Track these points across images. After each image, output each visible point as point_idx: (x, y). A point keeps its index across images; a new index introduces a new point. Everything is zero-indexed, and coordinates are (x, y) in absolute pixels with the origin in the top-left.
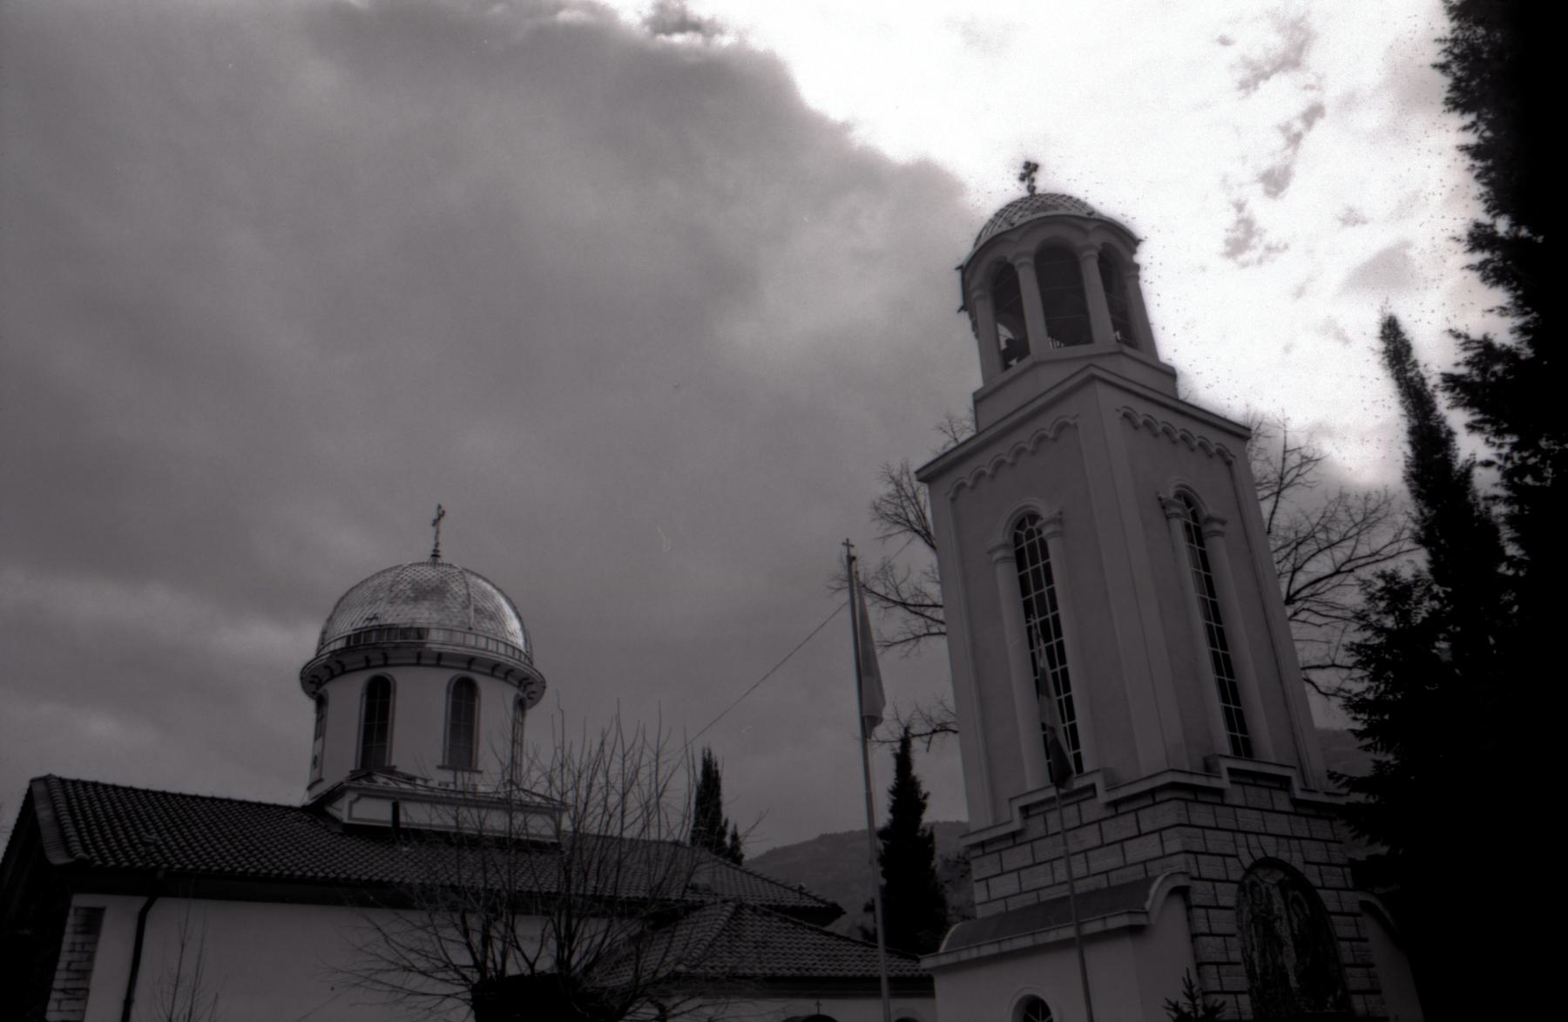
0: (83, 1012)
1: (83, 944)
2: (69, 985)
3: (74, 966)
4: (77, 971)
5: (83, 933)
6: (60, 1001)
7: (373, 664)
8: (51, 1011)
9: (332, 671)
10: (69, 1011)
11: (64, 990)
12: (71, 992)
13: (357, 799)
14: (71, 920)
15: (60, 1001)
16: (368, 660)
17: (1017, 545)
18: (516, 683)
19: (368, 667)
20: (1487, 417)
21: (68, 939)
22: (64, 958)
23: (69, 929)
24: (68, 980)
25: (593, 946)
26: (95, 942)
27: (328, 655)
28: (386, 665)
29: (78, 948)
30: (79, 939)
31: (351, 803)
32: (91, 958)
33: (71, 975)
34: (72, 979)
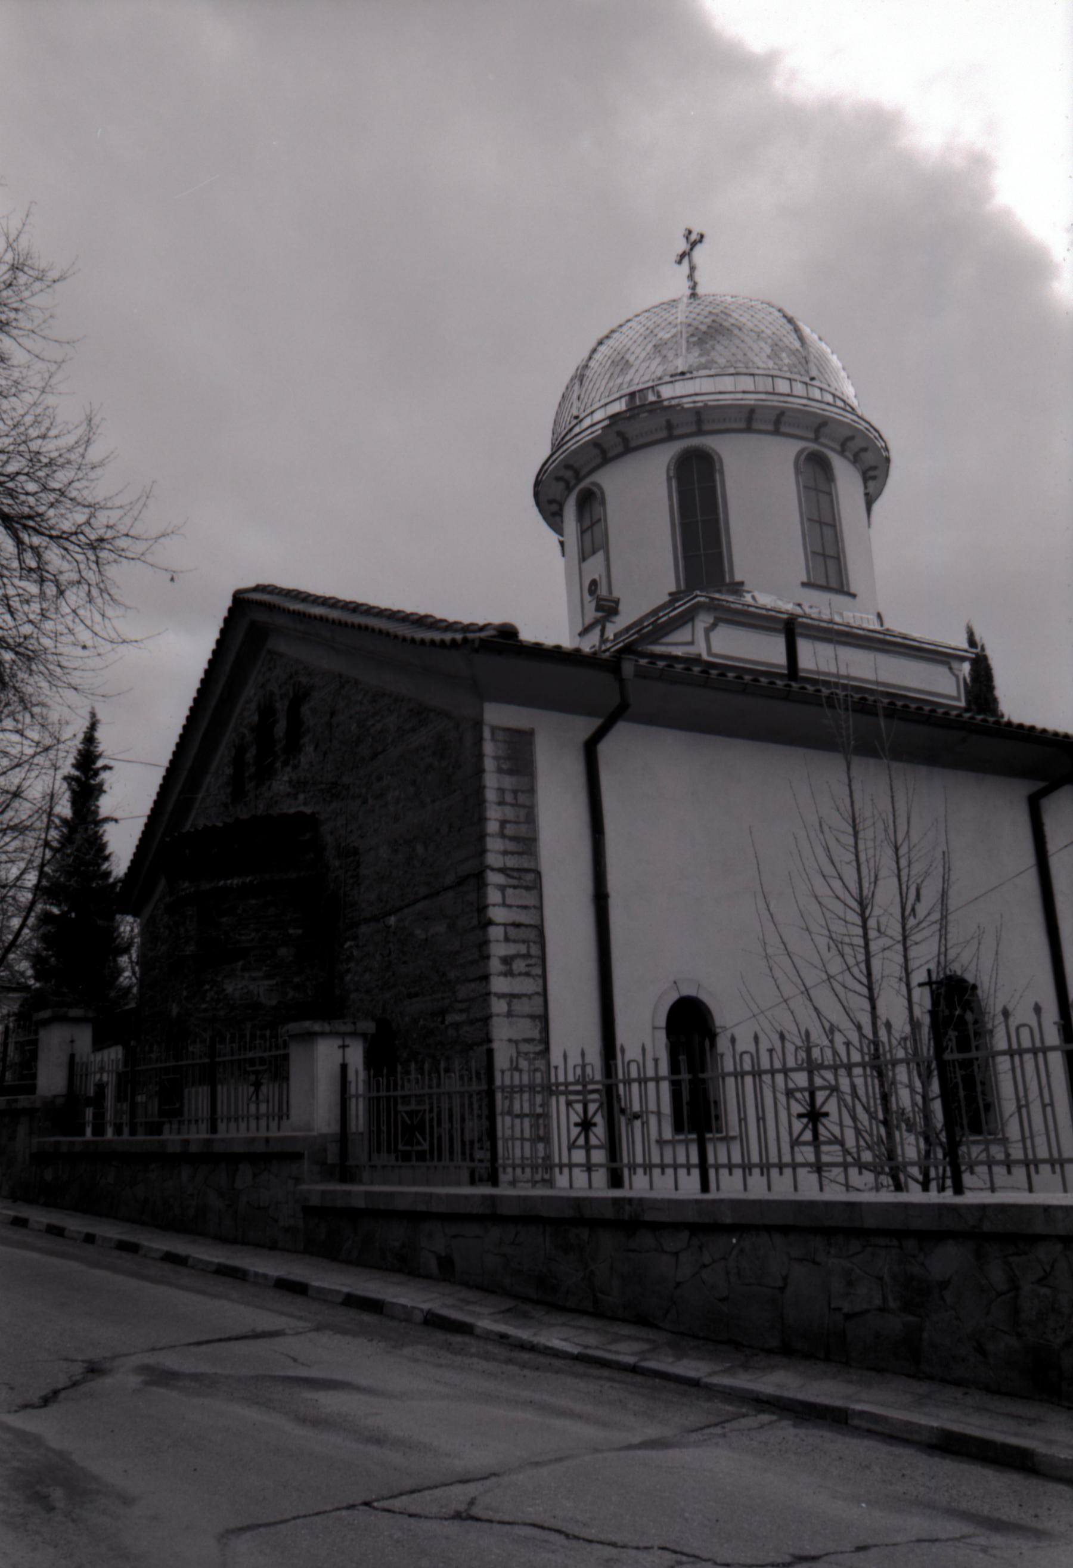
0: (540, 908)
1: (515, 792)
2: (511, 862)
3: (510, 830)
4: (515, 839)
5: (511, 772)
6: (502, 888)
7: (677, 432)
8: (835, 650)
9: (603, 452)
10: (518, 907)
11: (502, 870)
12: (515, 874)
13: (714, 626)
14: (489, 748)
15: (502, 888)
16: (669, 426)
17: (821, 705)
18: (851, 458)
19: (671, 438)
20: (946, 1146)
21: (491, 781)
22: (494, 814)
23: (489, 764)
24: (505, 853)
25: (718, 1368)
26: (532, 791)
27: (606, 423)
28: (700, 432)
29: (509, 798)
30: (508, 782)
31: (708, 631)
32: (531, 818)
33: (511, 846)
34: (512, 853)
